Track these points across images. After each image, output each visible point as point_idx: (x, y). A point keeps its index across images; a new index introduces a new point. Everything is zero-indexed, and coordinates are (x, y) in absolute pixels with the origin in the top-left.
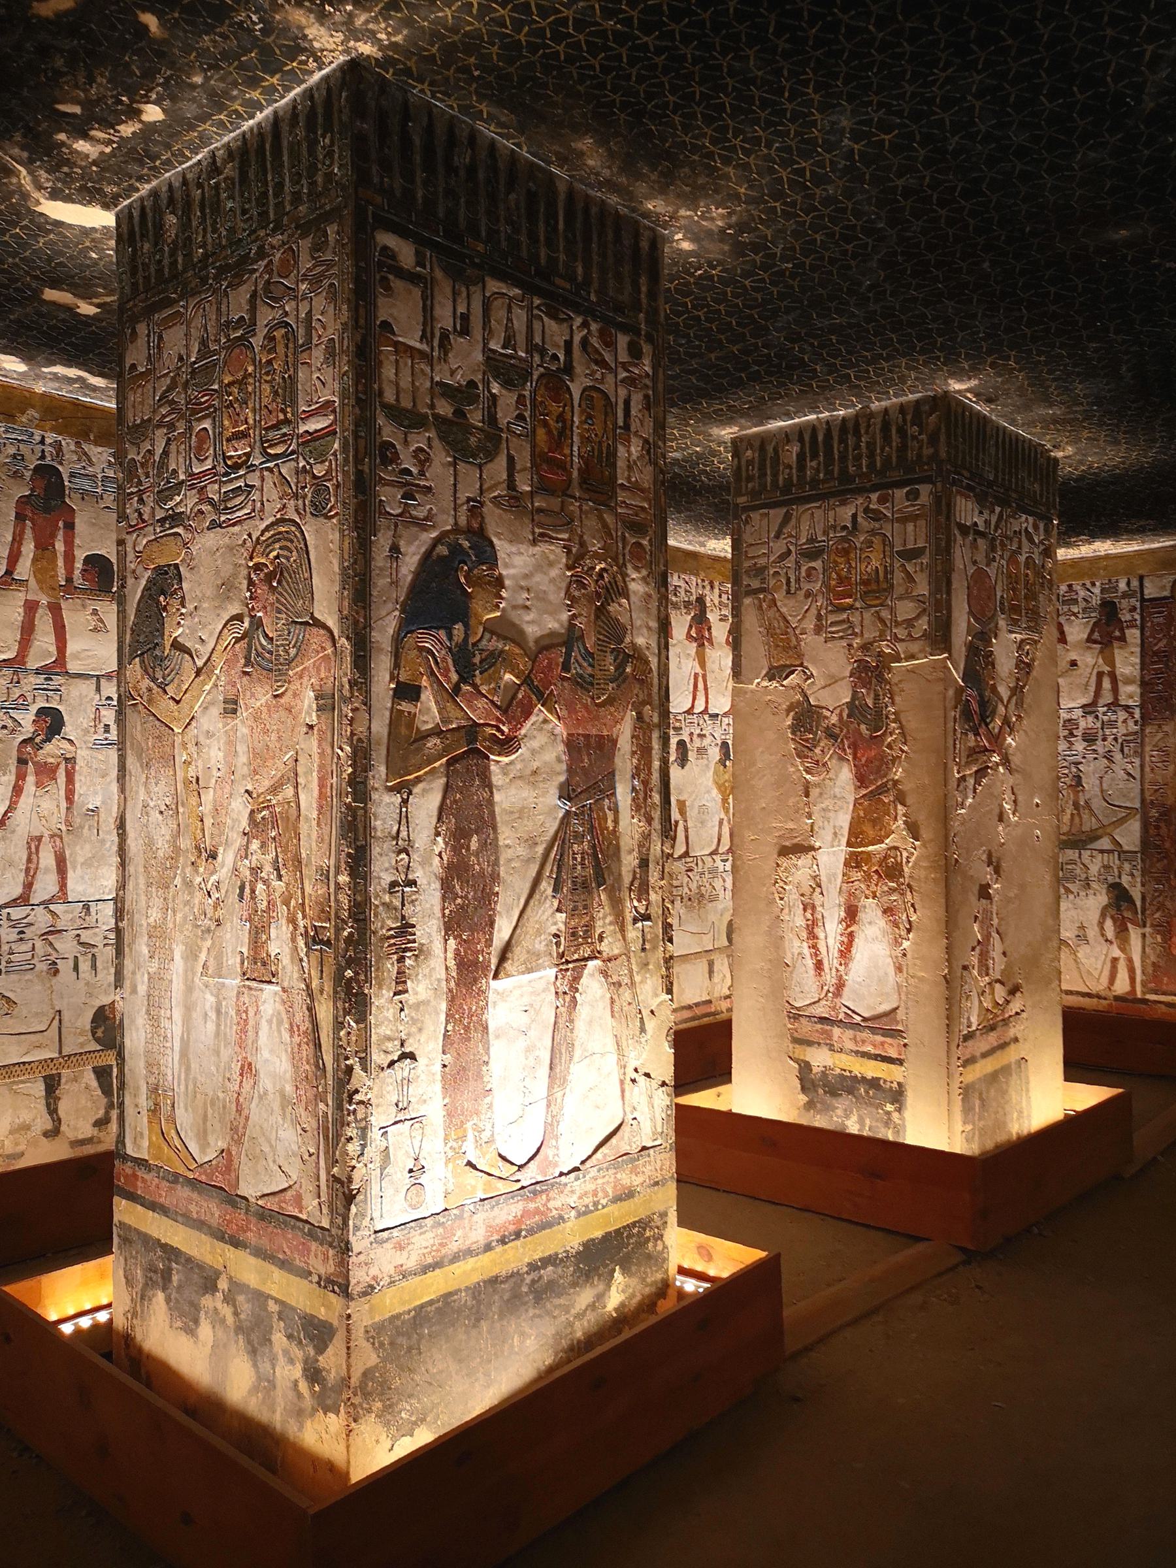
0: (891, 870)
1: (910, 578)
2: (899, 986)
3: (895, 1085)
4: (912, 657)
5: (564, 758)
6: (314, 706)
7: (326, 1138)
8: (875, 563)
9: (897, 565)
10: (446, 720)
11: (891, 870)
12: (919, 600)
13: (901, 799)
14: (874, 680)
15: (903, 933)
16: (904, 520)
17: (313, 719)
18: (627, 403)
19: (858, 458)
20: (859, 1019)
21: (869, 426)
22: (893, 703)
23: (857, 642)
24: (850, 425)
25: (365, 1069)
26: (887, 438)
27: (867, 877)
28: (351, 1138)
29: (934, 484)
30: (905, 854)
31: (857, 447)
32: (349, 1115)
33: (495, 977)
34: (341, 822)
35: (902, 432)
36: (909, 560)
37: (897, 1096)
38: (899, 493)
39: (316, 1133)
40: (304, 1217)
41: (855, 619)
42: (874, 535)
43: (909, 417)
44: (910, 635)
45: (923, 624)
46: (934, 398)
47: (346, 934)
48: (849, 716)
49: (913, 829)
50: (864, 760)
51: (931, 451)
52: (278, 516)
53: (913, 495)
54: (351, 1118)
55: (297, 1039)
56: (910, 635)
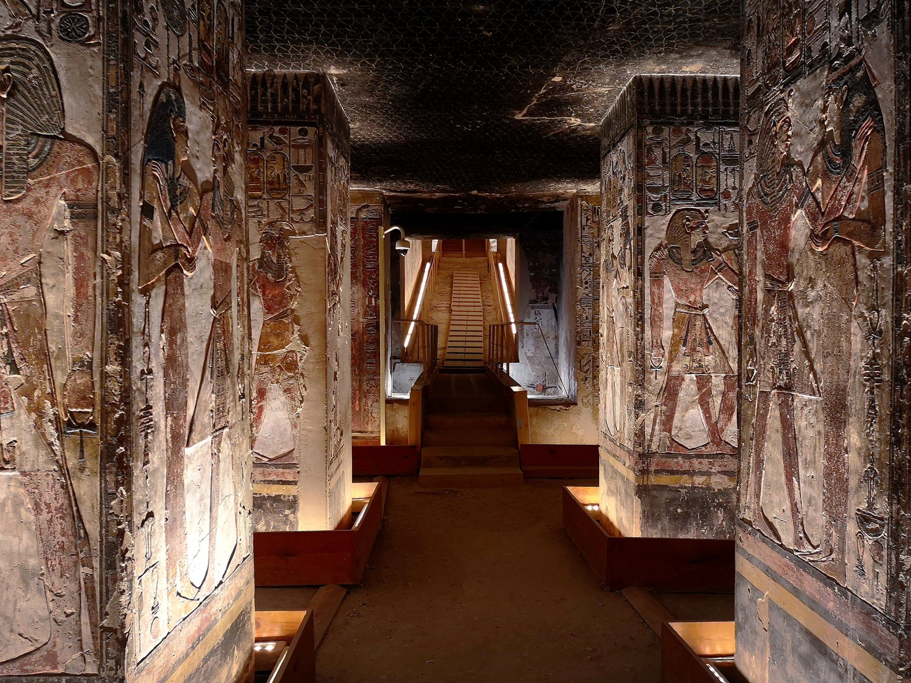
0: (290, 365)
1: (301, 184)
2: (294, 437)
3: (291, 497)
4: (304, 233)
5: (213, 277)
6: (67, 214)
7: (91, 596)
8: (277, 171)
9: (292, 175)
10: (165, 239)
11: (290, 365)
12: (307, 198)
13: (296, 320)
14: (277, 246)
15: (298, 403)
16: (298, 147)
17: (67, 224)
18: (233, 19)
19: (265, 102)
20: (266, 460)
21: (272, 84)
22: (291, 261)
23: (264, 220)
24: (260, 79)
25: (131, 531)
26: (285, 93)
27: (273, 371)
28: (124, 591)
29: (318, 128)
30: (299, 355)
31: (264, 94)
32: (122, 571)
33: (188, 445)
34: (109, 318)
35: (295, 90)
36: (301, 172)
37: (293, 504)
38: (295, 130)
39: (76, 595)
40: (60, 670)
41: (263, 205)
42: (277, 153)
43: (301, 84)
44: (302, 219)
45: (311, 213)
46: (318, 75)
47: (117, 416)
48: (259, 268)
49: (305, 339)
50: (270, 296)
51: (316, 107)
52: (9, 32)
53: (304, 133)
54: (124, 574)
55: (45, 516)
56: (302, 219)
